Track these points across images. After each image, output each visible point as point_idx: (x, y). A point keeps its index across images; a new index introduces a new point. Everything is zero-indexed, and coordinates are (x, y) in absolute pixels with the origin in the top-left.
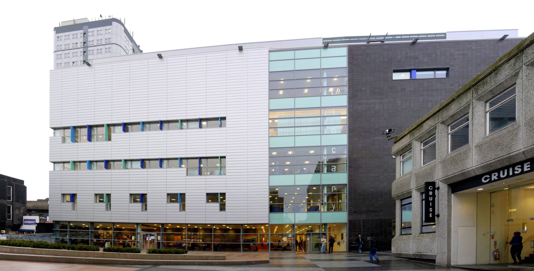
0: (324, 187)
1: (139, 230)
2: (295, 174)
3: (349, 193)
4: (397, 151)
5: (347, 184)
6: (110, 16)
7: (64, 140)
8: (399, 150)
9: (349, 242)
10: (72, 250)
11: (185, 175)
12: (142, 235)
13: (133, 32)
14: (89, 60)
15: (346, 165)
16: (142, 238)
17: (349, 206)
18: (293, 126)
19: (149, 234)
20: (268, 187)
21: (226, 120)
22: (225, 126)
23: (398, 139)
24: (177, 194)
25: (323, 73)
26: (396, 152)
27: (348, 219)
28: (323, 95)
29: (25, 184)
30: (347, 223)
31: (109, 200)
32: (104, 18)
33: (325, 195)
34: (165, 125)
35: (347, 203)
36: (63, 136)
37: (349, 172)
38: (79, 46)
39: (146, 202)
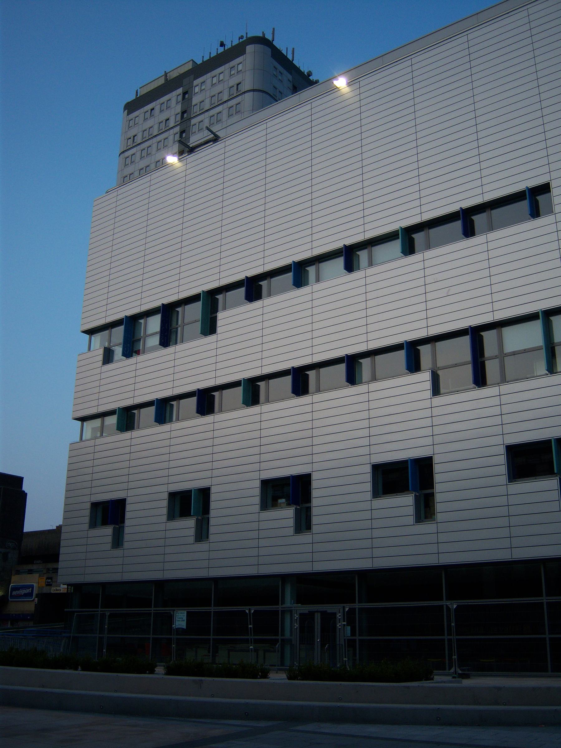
1: (289, 601)
6: (242, 37)
7: (108, 357)
10: (83, 670)
11: (429, 394)
12: (296, 616)
13: (293, 49)
14: (176, 153)
16: (296, 625)
19: (317, 612)
21: (550, 191)
22: (550, 211)
24: (189, 492)
29: (25, 488)
31: (206, 508)
32: (228, 46)
34: (363, 255)
36: (106, 345)
38: (172, 123)
39: (123, 521)
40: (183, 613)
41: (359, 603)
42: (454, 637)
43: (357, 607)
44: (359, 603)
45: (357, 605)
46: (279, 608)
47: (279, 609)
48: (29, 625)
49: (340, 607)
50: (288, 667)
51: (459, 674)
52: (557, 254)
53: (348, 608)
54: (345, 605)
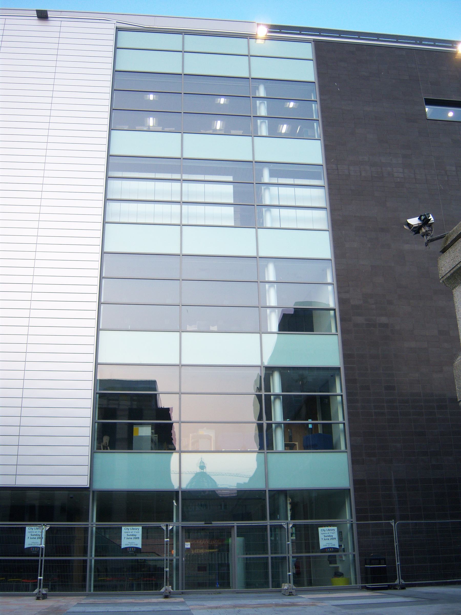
0: (272, 374)
2: (181, 331)
3: (348, 394)
4: (452, 272)
5: (339, 369)
8: (454, 269)
9: (360, 555)
15: (332, 312)
17: (351, 436)
18: (178, 199)
20: (90, 385)
23: (449, 242)
25: (257, 88)
26: (449, 275)
27: (352, 478)
28: (259, 134)
30: (349, 489)
33: (276, 427)
35: (344, 424)
37: (352, 450)
40: (136, 529)
41: (271, 519)
42: (44, 558)
43: (236, 524)
44: (271, 519)
45: (268, 522)
46: (88, 525)
47: (88, 526)
48: (77, 539)
49: (285, 523)
50: (387, 586)
51: (43, 594)
52: (3, 50)
53: (48, 527)
54: (168, 523)
